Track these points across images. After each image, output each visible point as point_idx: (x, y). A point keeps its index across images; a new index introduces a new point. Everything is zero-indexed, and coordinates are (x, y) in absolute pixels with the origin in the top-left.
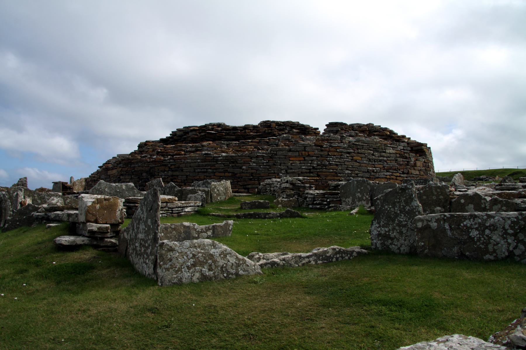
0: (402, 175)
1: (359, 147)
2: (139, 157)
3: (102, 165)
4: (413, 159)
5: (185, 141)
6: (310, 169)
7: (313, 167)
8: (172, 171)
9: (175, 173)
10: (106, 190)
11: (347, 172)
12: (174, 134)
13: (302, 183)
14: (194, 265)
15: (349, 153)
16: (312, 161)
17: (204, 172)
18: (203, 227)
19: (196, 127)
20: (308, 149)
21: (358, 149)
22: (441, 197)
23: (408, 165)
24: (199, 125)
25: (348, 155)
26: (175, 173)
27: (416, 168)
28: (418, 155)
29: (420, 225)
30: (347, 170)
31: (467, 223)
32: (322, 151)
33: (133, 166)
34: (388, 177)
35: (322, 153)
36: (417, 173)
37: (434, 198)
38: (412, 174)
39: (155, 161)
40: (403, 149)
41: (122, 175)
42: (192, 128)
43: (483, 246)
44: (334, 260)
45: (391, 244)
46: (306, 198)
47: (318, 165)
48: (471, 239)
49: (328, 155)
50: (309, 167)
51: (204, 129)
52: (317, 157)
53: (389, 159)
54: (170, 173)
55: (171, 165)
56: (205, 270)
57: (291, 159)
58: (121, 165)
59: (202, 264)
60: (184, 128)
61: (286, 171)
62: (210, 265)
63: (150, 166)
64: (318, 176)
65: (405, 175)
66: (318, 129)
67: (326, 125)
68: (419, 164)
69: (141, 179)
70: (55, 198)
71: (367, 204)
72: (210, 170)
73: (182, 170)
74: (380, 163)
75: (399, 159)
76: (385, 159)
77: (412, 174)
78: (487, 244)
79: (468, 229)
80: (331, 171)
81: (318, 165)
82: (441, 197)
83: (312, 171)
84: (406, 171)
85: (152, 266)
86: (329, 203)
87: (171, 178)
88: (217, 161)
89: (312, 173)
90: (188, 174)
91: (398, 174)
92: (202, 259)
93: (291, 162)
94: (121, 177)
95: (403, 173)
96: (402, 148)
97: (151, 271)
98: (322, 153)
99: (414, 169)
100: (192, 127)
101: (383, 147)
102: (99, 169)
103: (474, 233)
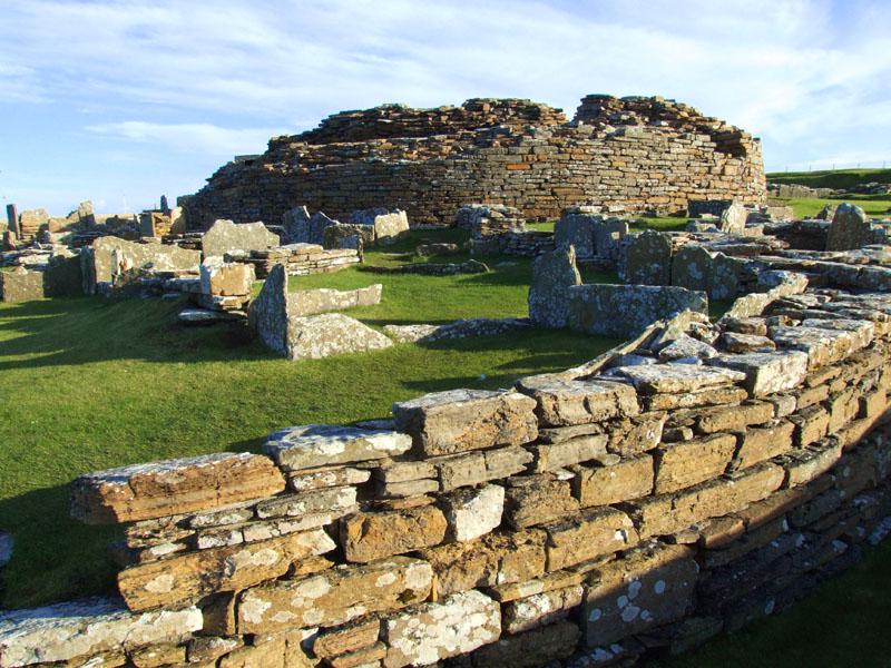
0: (697, 191)
1: (623, 145)
2: (271, 168)
3: (210, 176)
4: (720, 163)
5: (342, 137)
6: (540, 184)
7: (546, 181)
8: (323, 189)
9: (327, 194)
10: (225, 234)
11: (600, 187)
12: (326, 123)
13: (507, 216)
14: (323, 340)
15: (606, 156)
16: (544, 169)
17: (372, 191)
18: (345, 293)
19: (360, 112)
20: (537, 150)
21: (621, 148)
22: (660, 251)
23: (709, 172)
24: (364, 109)
25: (604, 159)
26: (327, 194)
27: (723, 177)
28: (730, 155)
29: (572, 296)
30: (601, 183)
31: (616, 296)
32: (560, 152)
33: (261, 181)
34: (672, 194)
35: (560, 157)
36: (727, 185)
37: (651, 251)
38: (715, 188)
39: (295, 174)
40: (704, 147)
41: (245, 197)
42: (354, 115)
43: (628, 322)
44: (479, 333)
45: (549, 315)
46: (510, 239)
47: (553, 176)
48: (619, 313)
49: (571, 159)
50: (539, 181)
51: (372, 114)
52: (552, 163)
53: (675, 163)
54: (320, 193)
55: (321, 180)
56: (335, 345)
57: (509, 167)
58: (243, 181)
59: (331, 339)
60: (342, 113)
61: (502, 187)
62: (339, 340)
63: (290, 182)
64: (553, 194)
65: (703, 191)
66: (561, 110)
67: (582, 100)
68: (729, 170)
69: (276, 203)
70: (161, 255)
71: (589, 251)
72: (381, 188)
73: (339, 188)
74: (658, 171)
75: (693, 164)
76: (669, 163)
77: (715, 188)
78: (632, 320)
79: (617, 304)
80: (575, 185)
81: (553, 176)
82: (660, 251)
83: (543, 185)
84: (704, 184)
85: (282, 341)
86: (537, 249)
87: (321, 201)
88: (392, 173)
89: (544, 189)
90: (348, 194)
91: (691, 190)
92: (330, 333)
93: (510, 172)
94: (244, 200)
95: (700, 186)
96: (701, 144)
97: (281, 346)
98: (560, 157)
99: (721, 180)
100: (356, 112)
101: (666, 144)
102: (207, 183)
103: (622, 307)
